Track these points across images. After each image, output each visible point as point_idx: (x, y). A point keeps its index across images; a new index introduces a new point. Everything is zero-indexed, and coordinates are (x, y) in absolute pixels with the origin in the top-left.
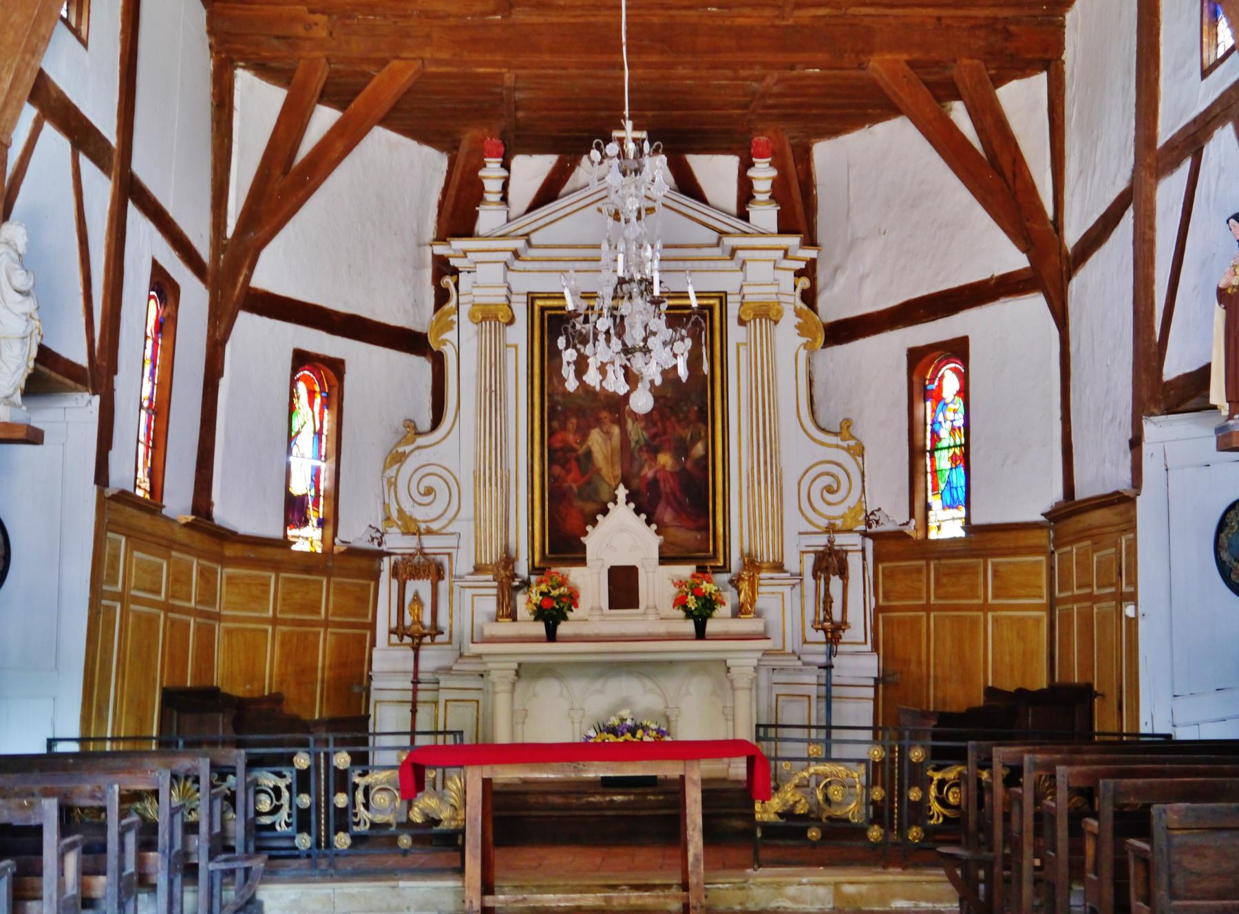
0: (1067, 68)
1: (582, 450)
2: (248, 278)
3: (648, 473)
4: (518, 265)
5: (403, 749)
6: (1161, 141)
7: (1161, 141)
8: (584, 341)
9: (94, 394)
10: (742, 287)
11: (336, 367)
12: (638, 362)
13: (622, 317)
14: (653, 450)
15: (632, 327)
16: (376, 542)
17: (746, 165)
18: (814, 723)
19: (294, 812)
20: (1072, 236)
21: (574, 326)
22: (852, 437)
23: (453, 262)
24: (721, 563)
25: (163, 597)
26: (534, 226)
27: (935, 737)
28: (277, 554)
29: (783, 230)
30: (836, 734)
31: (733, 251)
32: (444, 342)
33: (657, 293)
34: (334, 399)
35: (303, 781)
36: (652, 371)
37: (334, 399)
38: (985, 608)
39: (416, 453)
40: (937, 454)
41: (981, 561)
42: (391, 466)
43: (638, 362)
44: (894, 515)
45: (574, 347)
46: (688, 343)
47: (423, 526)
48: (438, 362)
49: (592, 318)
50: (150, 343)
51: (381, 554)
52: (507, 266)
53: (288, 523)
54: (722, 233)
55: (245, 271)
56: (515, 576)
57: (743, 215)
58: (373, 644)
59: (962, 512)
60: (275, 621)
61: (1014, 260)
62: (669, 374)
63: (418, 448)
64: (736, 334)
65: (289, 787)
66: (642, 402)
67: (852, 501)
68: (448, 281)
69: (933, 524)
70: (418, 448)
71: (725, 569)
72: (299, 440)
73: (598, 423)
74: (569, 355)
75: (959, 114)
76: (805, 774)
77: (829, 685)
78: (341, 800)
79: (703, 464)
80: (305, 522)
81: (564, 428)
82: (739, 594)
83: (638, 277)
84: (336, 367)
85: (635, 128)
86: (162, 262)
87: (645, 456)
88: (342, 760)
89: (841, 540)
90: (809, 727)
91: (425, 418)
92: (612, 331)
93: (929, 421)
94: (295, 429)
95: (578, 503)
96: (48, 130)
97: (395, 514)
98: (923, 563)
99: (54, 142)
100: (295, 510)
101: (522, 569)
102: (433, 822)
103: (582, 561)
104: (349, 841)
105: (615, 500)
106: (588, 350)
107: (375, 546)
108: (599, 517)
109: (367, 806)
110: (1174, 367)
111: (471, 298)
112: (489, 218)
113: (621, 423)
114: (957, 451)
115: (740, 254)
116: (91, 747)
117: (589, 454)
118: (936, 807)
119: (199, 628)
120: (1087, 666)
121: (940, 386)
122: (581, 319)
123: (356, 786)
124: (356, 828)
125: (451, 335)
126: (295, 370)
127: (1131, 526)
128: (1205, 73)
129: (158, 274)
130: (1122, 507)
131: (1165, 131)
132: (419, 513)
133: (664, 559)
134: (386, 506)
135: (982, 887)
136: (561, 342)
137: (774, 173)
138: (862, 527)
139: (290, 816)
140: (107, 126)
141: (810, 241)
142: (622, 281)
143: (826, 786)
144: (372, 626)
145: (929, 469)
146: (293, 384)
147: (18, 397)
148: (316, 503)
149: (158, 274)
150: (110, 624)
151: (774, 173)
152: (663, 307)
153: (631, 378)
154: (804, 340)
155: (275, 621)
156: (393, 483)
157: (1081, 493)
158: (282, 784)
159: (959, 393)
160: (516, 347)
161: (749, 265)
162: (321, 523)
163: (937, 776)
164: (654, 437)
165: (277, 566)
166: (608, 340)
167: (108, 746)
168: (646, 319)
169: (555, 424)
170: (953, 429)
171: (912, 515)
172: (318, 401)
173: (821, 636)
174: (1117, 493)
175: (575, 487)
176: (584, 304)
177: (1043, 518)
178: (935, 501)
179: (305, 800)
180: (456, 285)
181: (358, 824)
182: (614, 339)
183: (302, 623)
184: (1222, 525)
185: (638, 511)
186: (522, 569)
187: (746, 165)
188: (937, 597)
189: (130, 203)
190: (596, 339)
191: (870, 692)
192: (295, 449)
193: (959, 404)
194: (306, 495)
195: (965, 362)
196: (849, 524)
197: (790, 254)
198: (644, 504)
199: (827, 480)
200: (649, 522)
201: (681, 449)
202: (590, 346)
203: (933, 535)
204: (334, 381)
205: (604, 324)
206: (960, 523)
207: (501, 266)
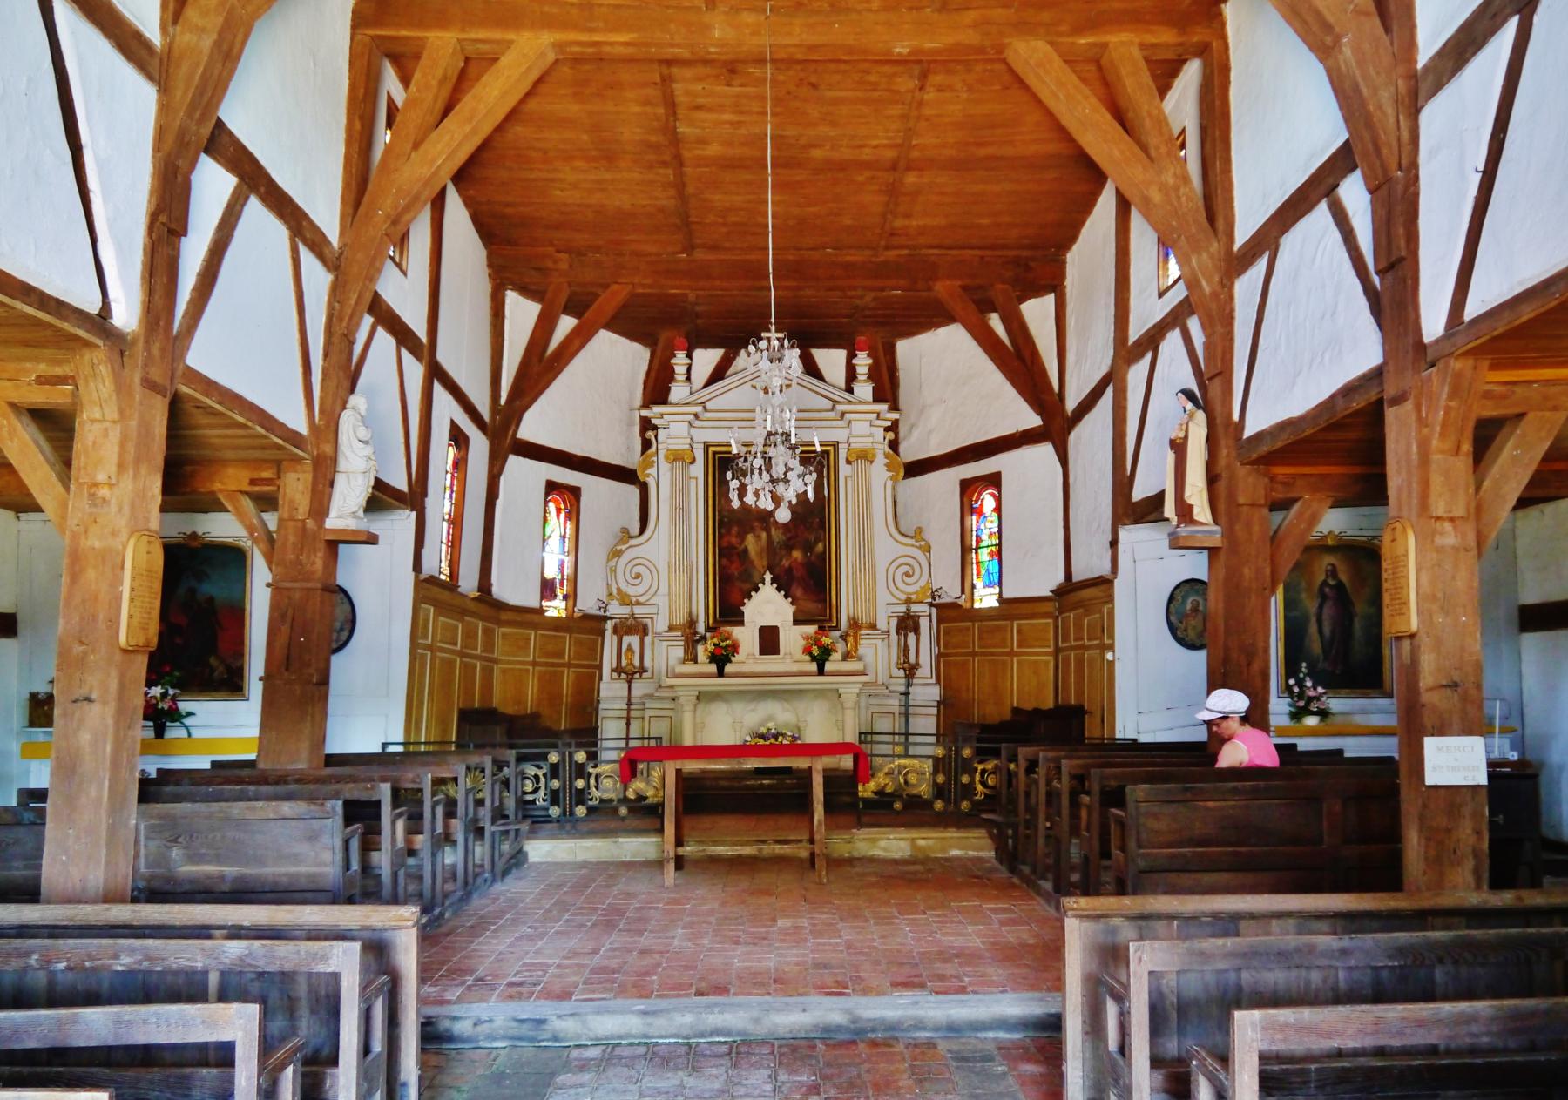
0: (1068, 290)
1: (741, 548)
2: (516, 432)
3: (786, 563)
4: (697, 423)
5: (622, 749)
6: (1132, 340)
7: (1132, 340)
8: (744, 475)
9: (412, 510)
11: (575, 492)
12: (781, 488)
13: (770, 458)
14: (789, 547)
15: (777, 465)
17: (851, 356)
19: (548, 792)
20: (1071, 404)
21: (737, 464)
23: (653, 421)
24: (834, 625)
25: (459, 647)
26: (708, 397)
27: (979, 740)
28: (536, 618)
29: (877, 399)
30: (911, 739)
31: (843, 414)
32: (648, 475)
33: (793, 442)
34: (574, 514)
35: (554, 771)
36: (790, 494)
37: (574, 514)
38: (1012, 654)
41: (1009, 622)
42: (613, 558)
43: (781, 488)
44: (951, 592)
45: (737, 479)
46: (815, 475)
47: (634, 600)
48: (644, 489)
49: (750, 459)
50: (449, 476)
52: (690, 424)
53: (542, 598)
54: (836, 402)
55: (513, 427)
56: (696, 633)
57: (850, 390)
58: (601, 678)
59: (997, 590)
60: (534, 664)
61: (1033, 420)
63: (631, 547)
64: (844, 470)
65: (545, 775)
66: (783, 515)
67: (922, 582)
68: (650, 434)
69: (976, 598)
70: (631, 547)
71: (837, 628)
72: (550, 541)
73: (752, 530)
74: (734, 484)
75: (995, 322)
76: (892, 766)
77: (907, 706)
78: (580, 784)
79: (823, 558)
80: (554, 597)
81: (729, 533)
83: (780, 431)
84: (575, 492)
85: (777, 331)
86: (456, 421)
87: (783, 552)
88: (580, 757)
89: (915, 608)
90: (894, 734)
91: (635, 527)
92: (763, 468)
93: (974, 529)
94: (547, 533)
95: (738, 584)
96: (380, 331)
97: (615, 592)
98: (970, 624)
99: (385, 341)
100: (548, 588)
101: (701, 628)
103: (741, 623)
104: (585, 812)
106: (747, 480)
108: (753, 593)
109: (597, 788)
110: (1140, 492)
111: (665, 445)
112: (678, 392)
114: (994, 549)
115: (847, 416)
116: (412, 748)
117: (746, 551)
118: (979, 788)
119: (483, 669)
120: (1080, 693)
121: (981, 505)
122: (742, 459)
123: (590, 774)
124: (590, 803)
125: (652, 471)
126: (547, 494)
127: (1110, 599)
128: (1161, 295)
129: (454, 427)
130: (1103, 587)
132: (631, 591)
133: (796, 622)
135: (1010, 841)
136: (729, 475)
137: (870, 361)
138: (930, 600)
139: (545, 794)
140: (420, 330)
141: (895, 407)
142: (770, 434)
144: (600, 667)
145: (974, 561)
147: (361, 513)
148: (562, 584)
149: (454, 427)
150: (423, 666)
151: (870, 361)
152: (798, 451)
153: (777, 500)
154: (891, 474)
156: (613, 571)
157: (1076, 577)
158: (540, 773)
159: (994, 510)
160: (697, 478)
162: (565, 597)
163: (980, 767)
164: (790, 539)
166: (760, 474)
167: (423, 748)
168: (786, 460)
170: (991, 534)
171: (963, 592)
172: (563, 515)
173: (902, 673)
174: (1101, 577)
175: (736, 573)
176: (745, 449)
177: (1051, 594)
178: (979, 583)
179: (556, 784)
180: (656, 437)
181: (591, 800)
182: (764, 473)
183: (553, 665)
184: (1171, 599)
185: (779, 589)
186: (701, 628)
187: (851, 356)
188: (980, 647)
189: (435, 381)
190: (752, 473)
191: (935, 711)
192: (547, 548)
194: (554, 579)
195: (1000, 492)
197: (881, 415)
198: (784, 584)
199: (906, 568)
200: (786, 597)
201: (808, 548)
202: (748, 477)
203: (977, 605)
204: (574, 502)
205: (758, 463)
206: (996, 597)
207: (687, 424)
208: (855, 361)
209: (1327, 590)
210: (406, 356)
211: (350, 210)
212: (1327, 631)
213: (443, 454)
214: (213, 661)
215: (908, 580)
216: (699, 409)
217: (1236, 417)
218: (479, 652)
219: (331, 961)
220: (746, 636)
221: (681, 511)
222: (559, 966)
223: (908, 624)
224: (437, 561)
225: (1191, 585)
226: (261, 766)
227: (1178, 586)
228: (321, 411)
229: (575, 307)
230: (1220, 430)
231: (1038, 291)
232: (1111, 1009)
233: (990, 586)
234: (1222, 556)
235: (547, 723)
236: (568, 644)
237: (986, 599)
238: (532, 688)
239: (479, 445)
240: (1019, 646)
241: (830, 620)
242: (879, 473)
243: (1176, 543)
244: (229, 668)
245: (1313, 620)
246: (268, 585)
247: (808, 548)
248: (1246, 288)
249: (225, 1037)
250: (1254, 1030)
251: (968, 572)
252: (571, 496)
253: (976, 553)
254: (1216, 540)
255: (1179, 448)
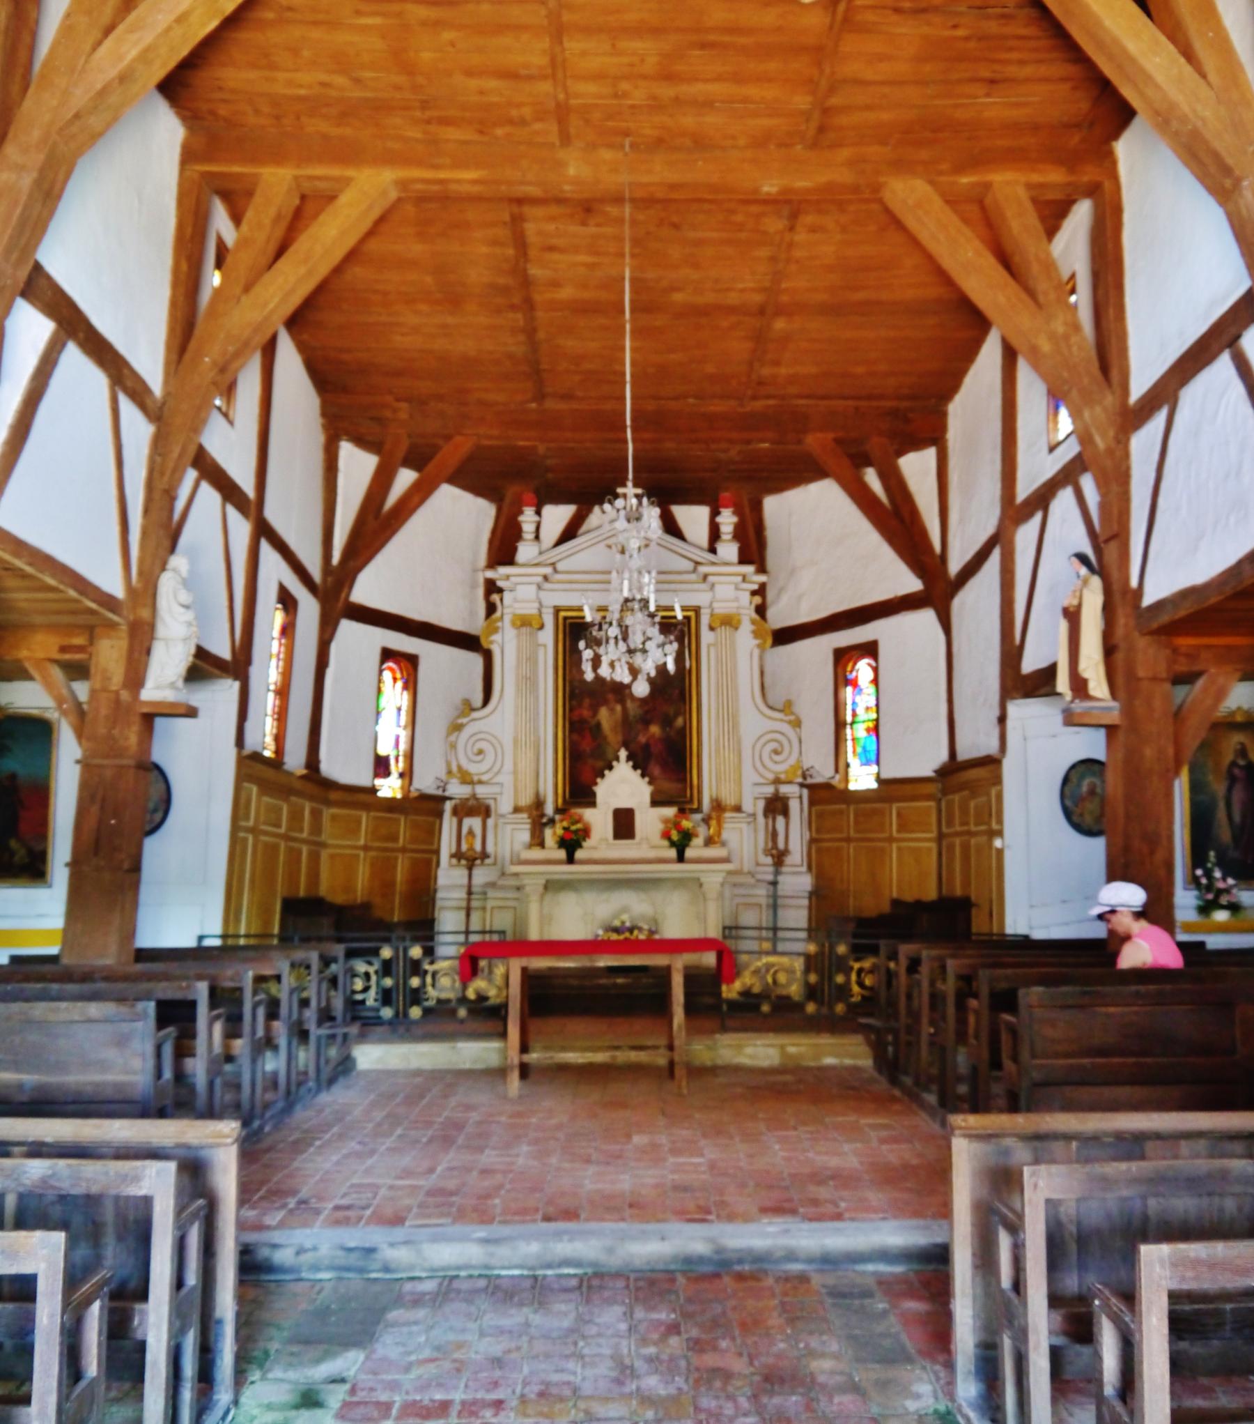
1: (593, 722)
3: (642, 739)
4: (547, 585)
10: (711, 603)
12: (638, 659)
13: (627, 627)
14: (646, 721)
16: (441, 789)
17: (715, 513)
18: (764, 925)
19: (380, 990)
20: (955, 566)
21: (591, 633)
22: (792, 713)
29: (743, 560)
31: (705, 577)
32: (492, 642)
34: (411, 684)
36: (649, 667)
38: (891, 839)
39: (472, 723)
40: (855, 726)
43: (638, 659)
44: (824, 772)
46: (675, 645)
49: (605, 627)
51: (444, 799)
52: (539, 587)
54: (697, 563)
55: (346, 590)
56: (543, 815)
57: (712, 550)
60: (366, 848)
61: (911, 584)
62: (662, 669)
64: (707, 637)
65: (376, 972)
66: (641, 689)
67: (792, 761)
68: (495, 597)
71: (699, 810)
73: (605, 702)
74: (587, 654)
75: (872, 478)
78: (415, 982)
82: (709, 828)
83: (638, 597)
88: (416, 952)
89: (785, 789)
91: (478, 699)
92: (620, 637)
97: (455, 769)
98: (844, 806)
99: (209, 496)
100: (381, 766)
101: (549, 809)
102: (482, 998)
105: (617, 759)
106: (601, 650)
107: (439, 792)
109: (433, 986)
110: (1031, 663)
112: (525, 551)
113: (622, 701)
115: (711, 579)
117: (598, 725)
120: (966, 883)
122: (597, 627)
123: (426, 972)
125: (496, 637)
126: (383, 661)
127: (997, 780)
130: (991, 767)
131: (1023, 491)
132: (473, 768)
133: (655, 803)
134: (448, 764)
135: (890, 1049)
136: (582, 644)
140: (248, 485)
141: (762, 569)
142: (627, 600)
143: (776, 972)
146: (381, 672)
147: (180, 683)
153: (634, 672)
155: (891, 839)
156: (453, 746)
160: (545, 646)
161: (717, 587)
162: (401, 775)
164: (646, 712)
165: (367, 807)
166: (616, 643)
169: (574, 703)
171: (837, 771)
173: (769, 860)
179: (388, 982)
180: (501, 600)
183: (386, 850)
184: (1066, 780)
185: (635, 767)
186: (549, 809)
187: (715, 513)
190: (607, 642)
191: (806, 902)
193: (872, 689)
196: (790, 777)
197: (747, 579)
198: (640, 762)
199: (773, 745)
200: (643, 776)
201: (667, 722)
204: (411, 672)
205: (614, 631)
208: (719, 519)
209: (1236, 771)
210: (232, 512)
211: (174, 357)
212: (1237, 818)
213: (271, 619)
214: (13, 844)
215: (777, 758)
216: (548, 570)
217: (1134, 583)
218: (305, 835)
219: (142, 1184)
220: (599, 819)
221: (528, 682)
222: (391, 1187)
223: (776, 806)
224: (263, 736)
225: (1088, 765)
226: (65, 961)
227: (1073, 767)
228: (141, 573)
229: (415, 460)
230: (1117, 597)
231: (916, 444)
232: (1004, 1241)
233: (867, 763)
234: (1121, 737)
235: (378, 913)
236: (403, 828)
237: (862, 778)
238: (362, 877)
239: (309, 608)
240: (899, 831)
241: (691, 801)
242: (746, 640)
243: (1070, 719)
244: (31, 852)
245: (1222, 805)
246: (78, 762)
247: (667, 722)
248: (1144, 442)
249: (25, 1269)
250: (1162, 1266)
251: (842, 750)
252: (408, 664)
253: (852, 728)
254: (1114, 717)
255: (1073, 616)
